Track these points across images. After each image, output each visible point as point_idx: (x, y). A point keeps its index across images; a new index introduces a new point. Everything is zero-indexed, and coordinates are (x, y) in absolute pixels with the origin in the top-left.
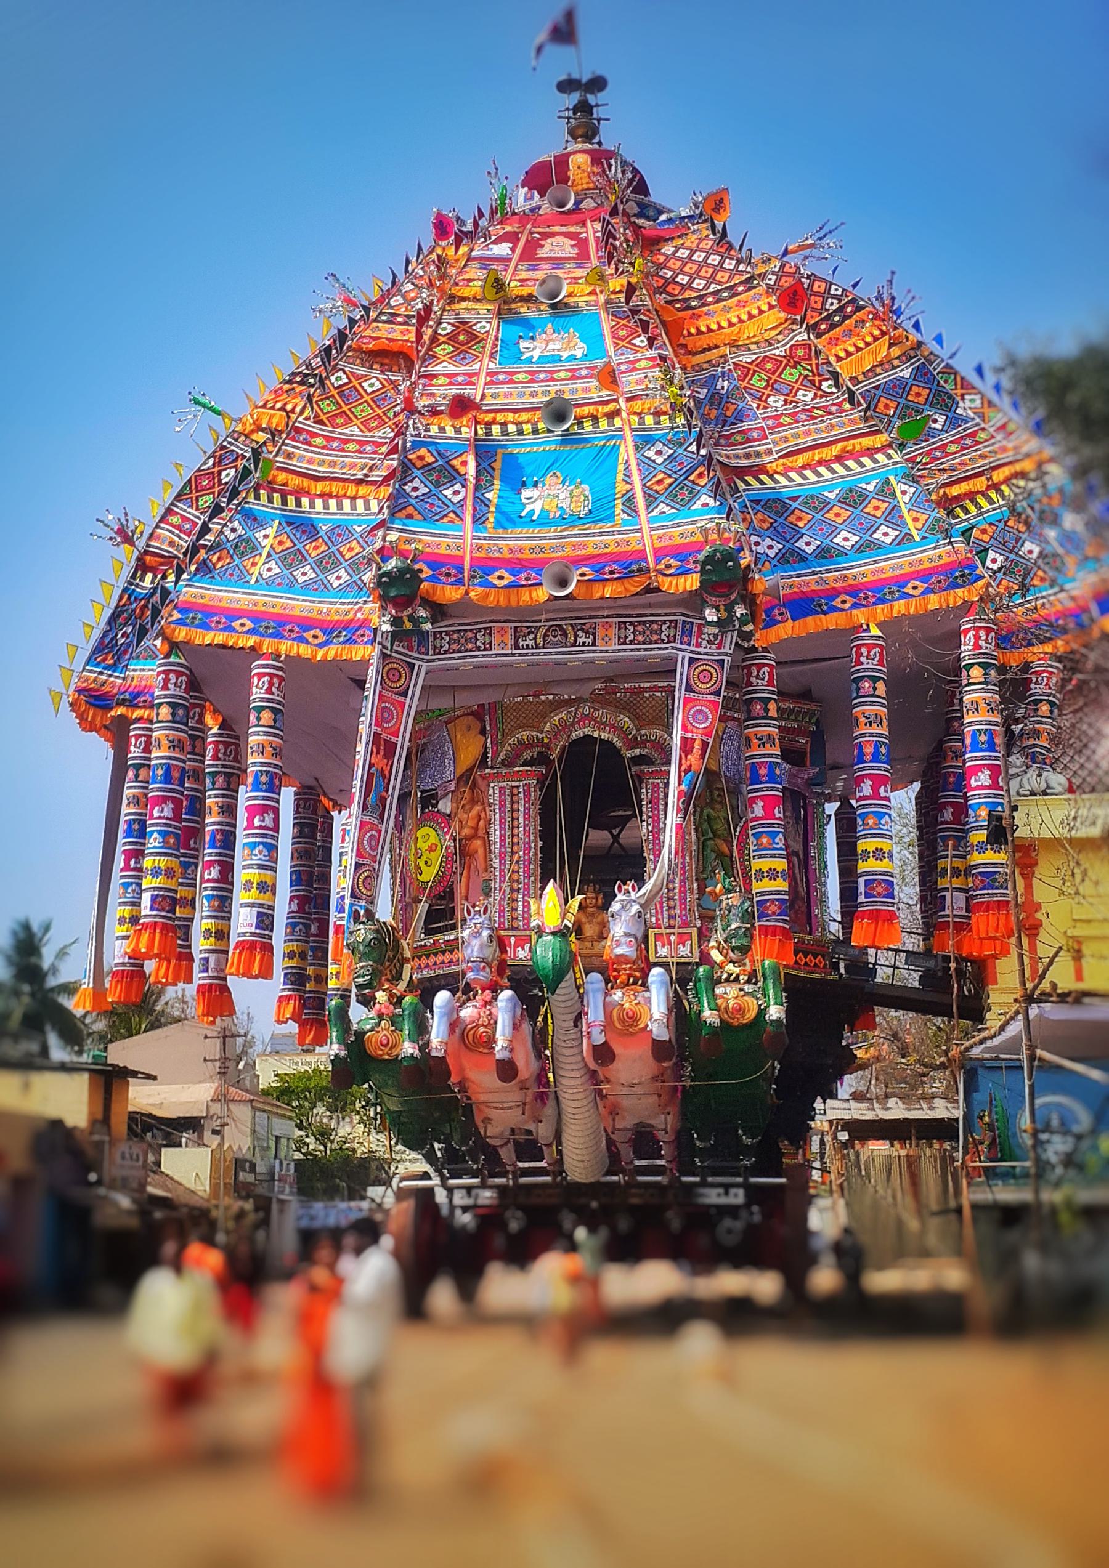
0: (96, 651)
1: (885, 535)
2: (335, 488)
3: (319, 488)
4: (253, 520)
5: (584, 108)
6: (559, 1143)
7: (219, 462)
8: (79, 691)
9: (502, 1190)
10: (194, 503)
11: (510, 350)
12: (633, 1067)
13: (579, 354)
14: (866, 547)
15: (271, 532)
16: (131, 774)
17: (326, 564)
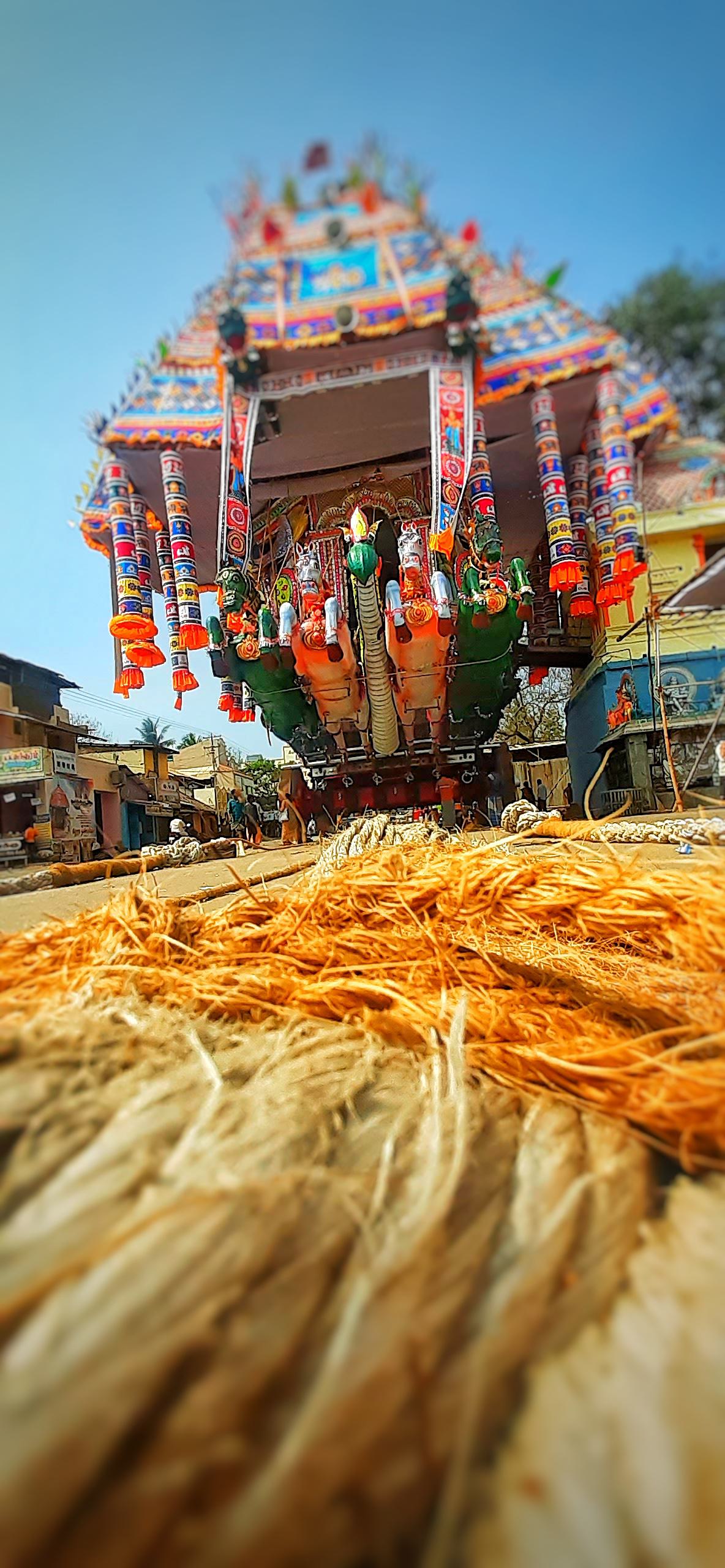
0: (93, 499)
1: (544, 339)
6: (370, 732)
9: (339, 766)
12: (425, 653)
14: (533, 346)
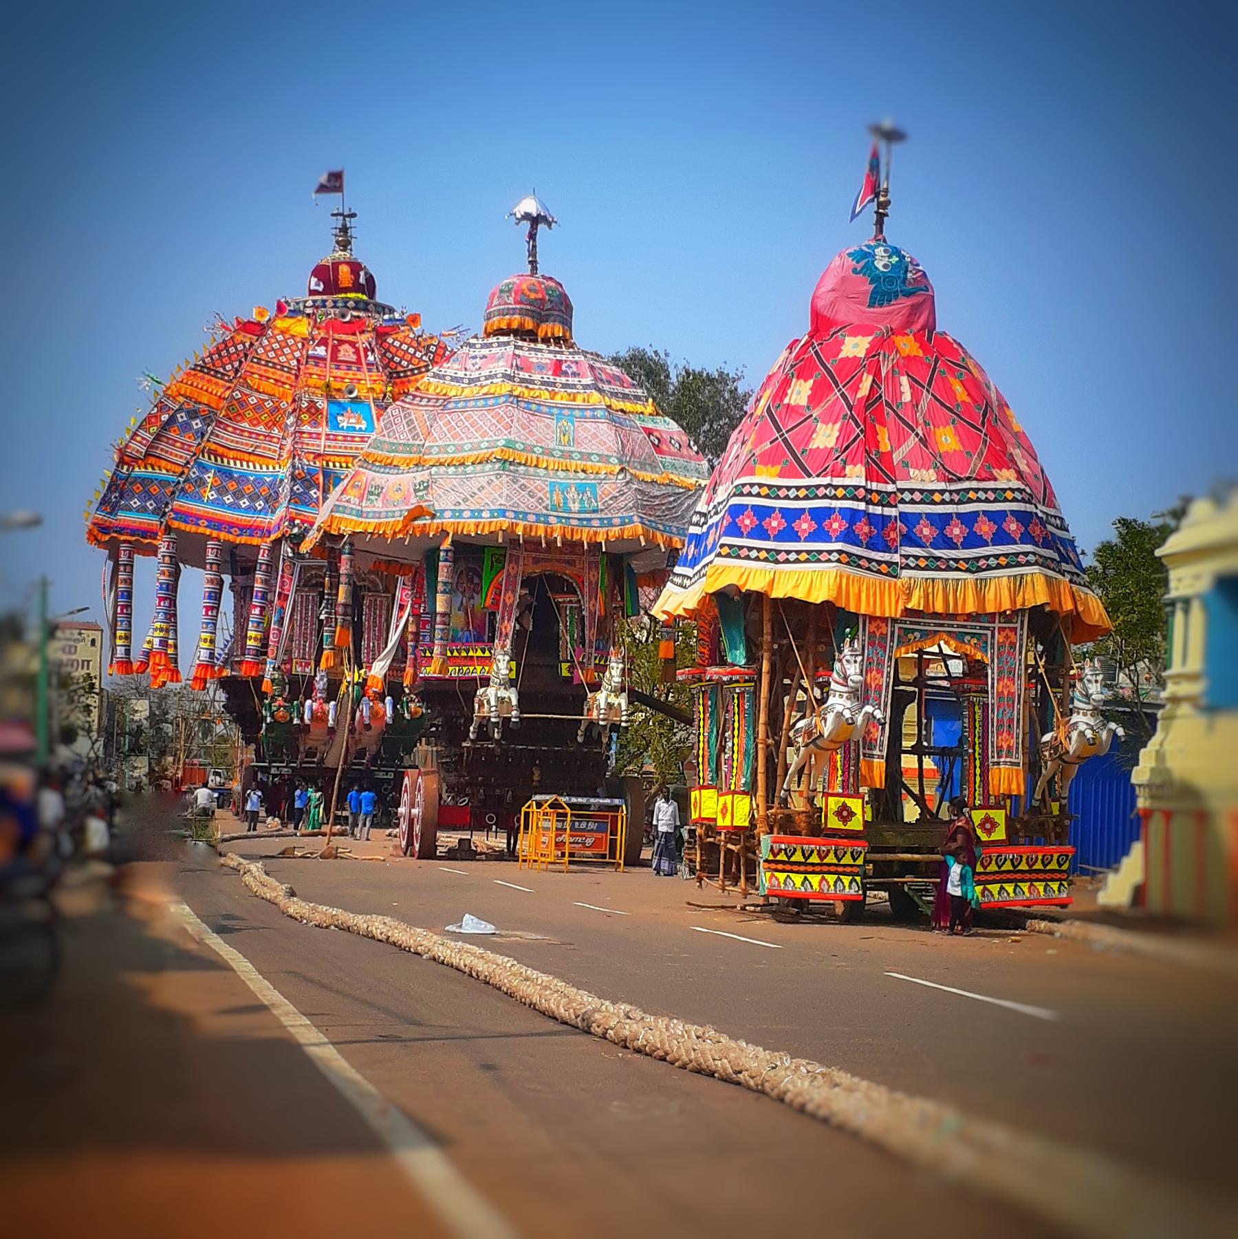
2: (239, 455)
3: (231, 454)
4: (205, 469)
5: (344, 229)
7: (160, 410)
8: (94, 524)
10: (148, 431)
11: (332, 421)
13: (363, 427)
15: (211, 475)
16: (122, 568)
17: (238, 495)
